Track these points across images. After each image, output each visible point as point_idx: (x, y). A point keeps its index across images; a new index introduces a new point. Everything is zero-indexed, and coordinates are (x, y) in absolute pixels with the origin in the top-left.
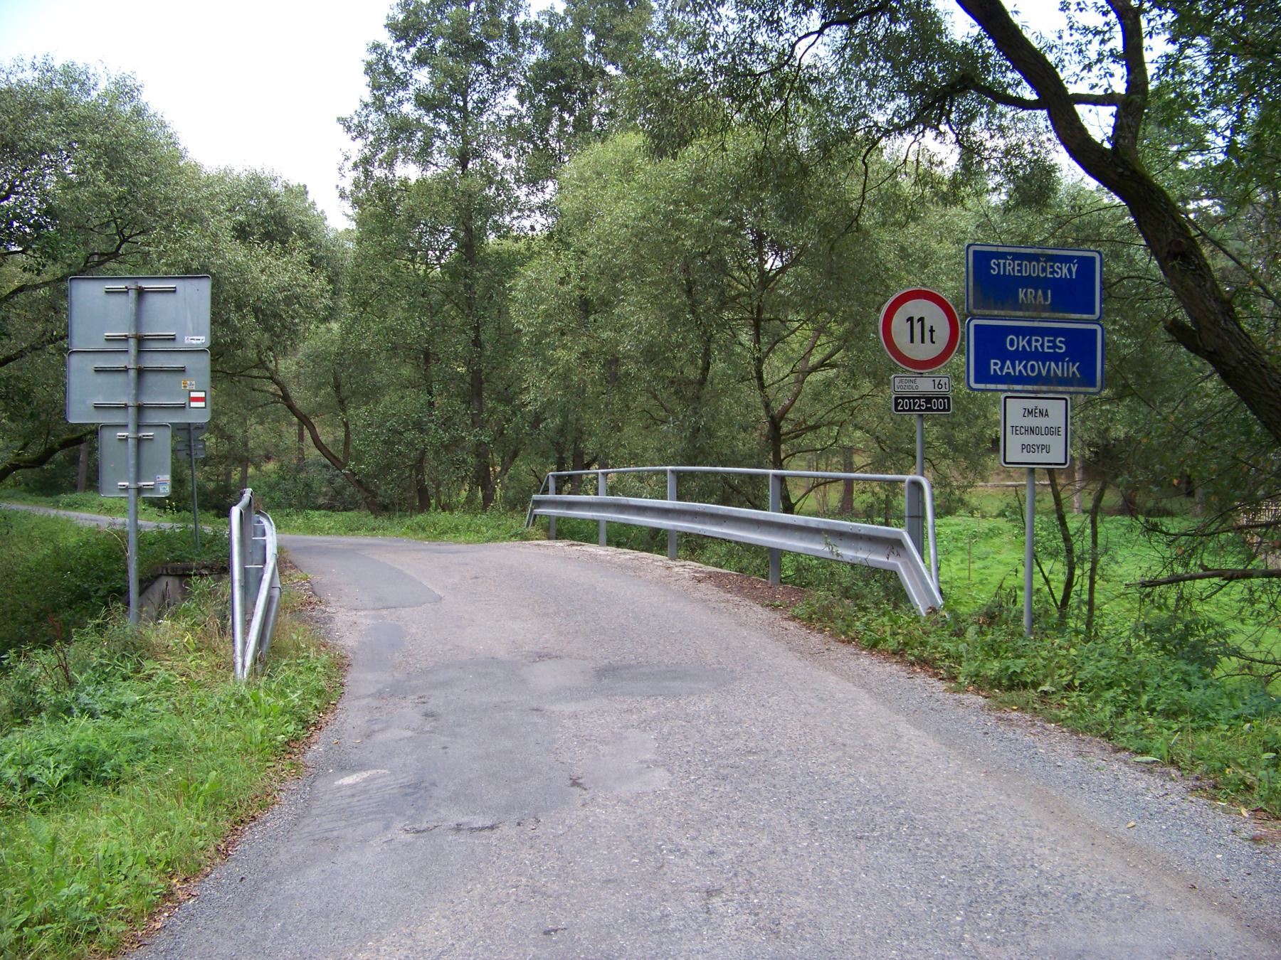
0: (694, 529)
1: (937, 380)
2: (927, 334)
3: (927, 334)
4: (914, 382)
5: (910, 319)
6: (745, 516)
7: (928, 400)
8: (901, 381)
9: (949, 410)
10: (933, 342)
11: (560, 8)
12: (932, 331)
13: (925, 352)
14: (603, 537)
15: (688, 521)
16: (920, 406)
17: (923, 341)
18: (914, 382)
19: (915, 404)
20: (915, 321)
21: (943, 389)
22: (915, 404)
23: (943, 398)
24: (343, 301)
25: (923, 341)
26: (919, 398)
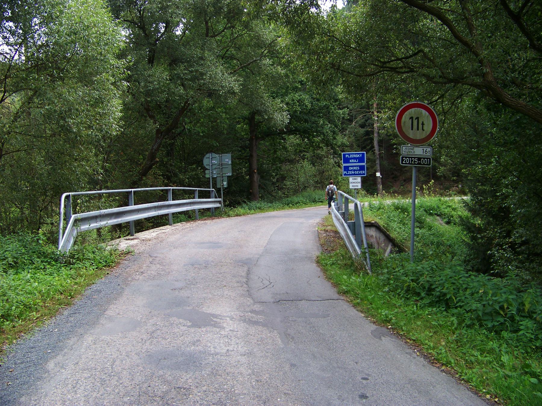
0: (124, 220)
1: (425, 149)
2: (420, 126)
3: (420, 126)
4: (413, 149)
5: (412, 118)
6: (86, 216)
7: (419, 159)
8: (406, 149)
9: (430, 165)
10: (423, 130)
11: (340, 5)
12: (423, 124)
13: (419, 135)
14: (170, 217)
15: (135, 215)
16: (415, 162)
17: (418, 129)
18: (413, 149)
19: (412, 161)
20: (414, 119)
21: (428, 154)
22: (412, 161)
23: (427, 158)
24: (533, 170)
25: (418, 129)
26: (415, 158)
